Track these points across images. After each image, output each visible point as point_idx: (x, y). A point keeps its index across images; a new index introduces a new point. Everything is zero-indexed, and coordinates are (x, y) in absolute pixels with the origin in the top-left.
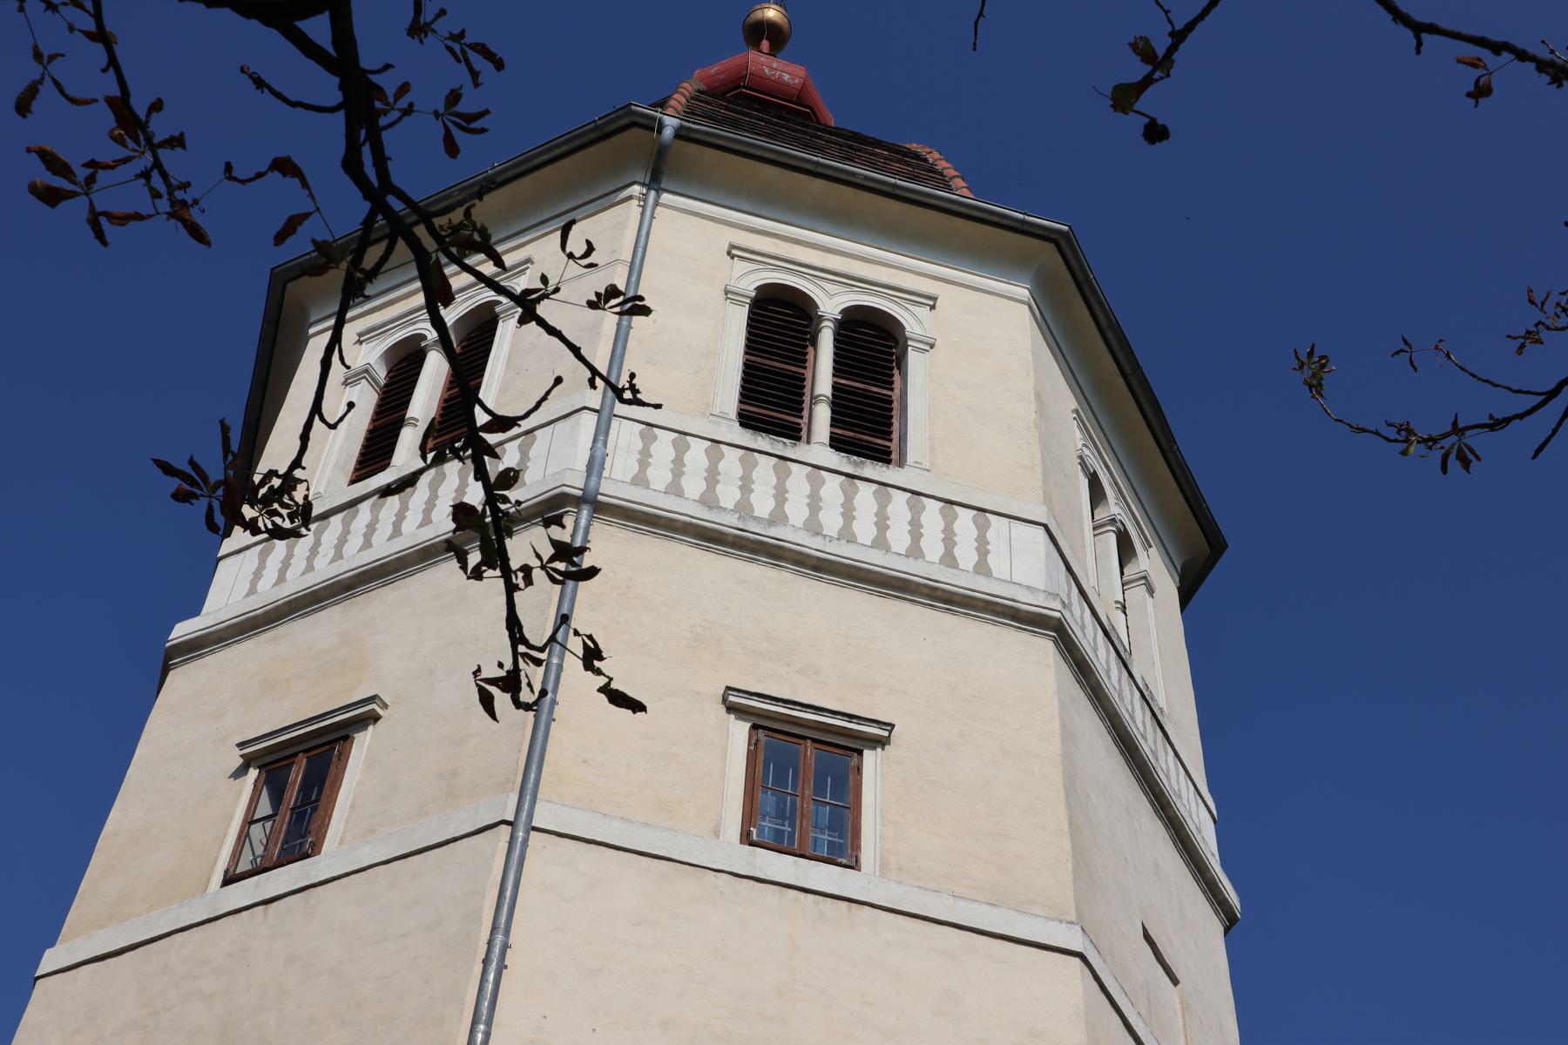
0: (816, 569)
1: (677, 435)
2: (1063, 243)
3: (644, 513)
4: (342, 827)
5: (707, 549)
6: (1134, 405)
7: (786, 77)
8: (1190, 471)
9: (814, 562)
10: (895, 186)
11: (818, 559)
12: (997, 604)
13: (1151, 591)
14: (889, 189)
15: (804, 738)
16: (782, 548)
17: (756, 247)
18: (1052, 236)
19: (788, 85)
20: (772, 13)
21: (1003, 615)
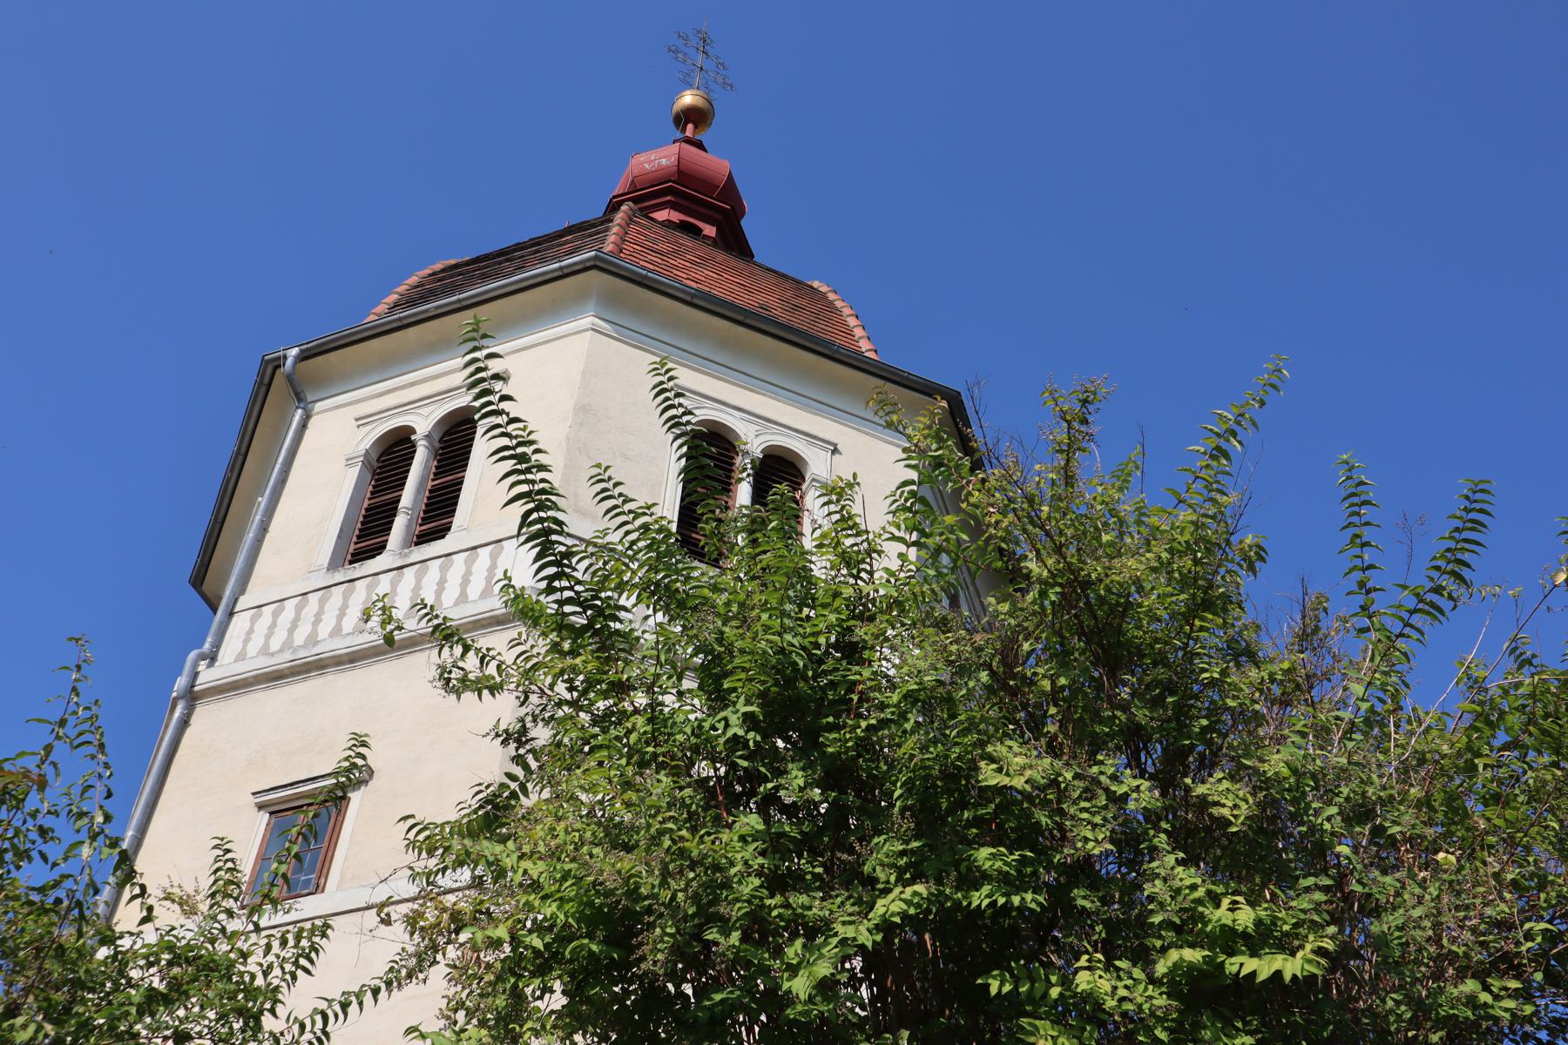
0: (352, 661)
1: (321, 592)
2: (599, 264)
3: (227, 684)
4: (876, 840)
5: (274, 687)
6: (769, 340)
7: (664, 161)
8: (264, 529)
9: (346, 658)
10: (459, 301)
11: (347, 654)
12: (479, 620)
13: (506, 571)
14: (399, 324)
15: (302, 806)
16: (321, 660)
17: (417, 397)
18: (588, 264)
19: (667, 167)
20: (688, 99)
21: (491, 625)
